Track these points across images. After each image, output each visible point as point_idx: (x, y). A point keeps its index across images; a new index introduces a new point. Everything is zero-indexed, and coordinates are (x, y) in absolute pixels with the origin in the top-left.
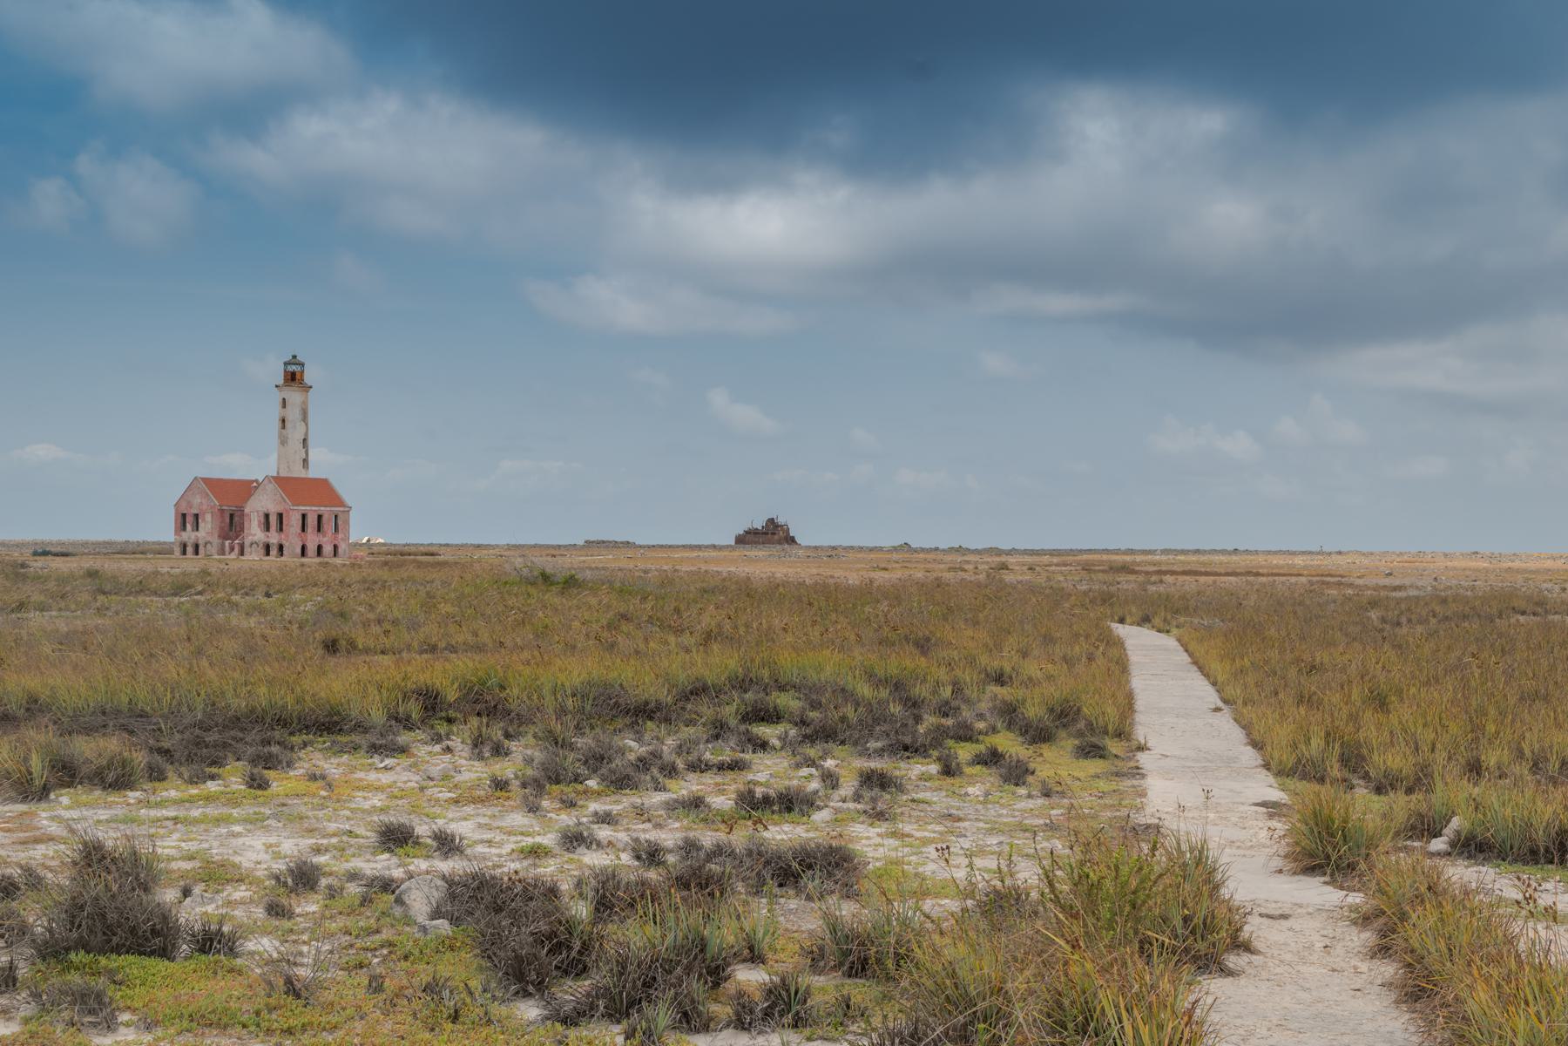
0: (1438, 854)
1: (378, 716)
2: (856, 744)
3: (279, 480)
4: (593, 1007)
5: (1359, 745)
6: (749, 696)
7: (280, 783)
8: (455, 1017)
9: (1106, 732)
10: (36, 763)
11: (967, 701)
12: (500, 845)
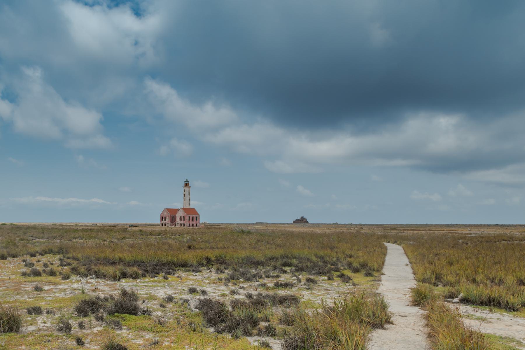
0: (456, 303)
1: (195, 263)
2: (309, 272)
3: (184, 209)
4: (225, 330)
5: (441, 274)
6: (284, 260)
7: (170, 278)
8: (195, 330)
9: (374, 270)
10: (117, 273)
11: (340, 262)
12: (217, 293)
